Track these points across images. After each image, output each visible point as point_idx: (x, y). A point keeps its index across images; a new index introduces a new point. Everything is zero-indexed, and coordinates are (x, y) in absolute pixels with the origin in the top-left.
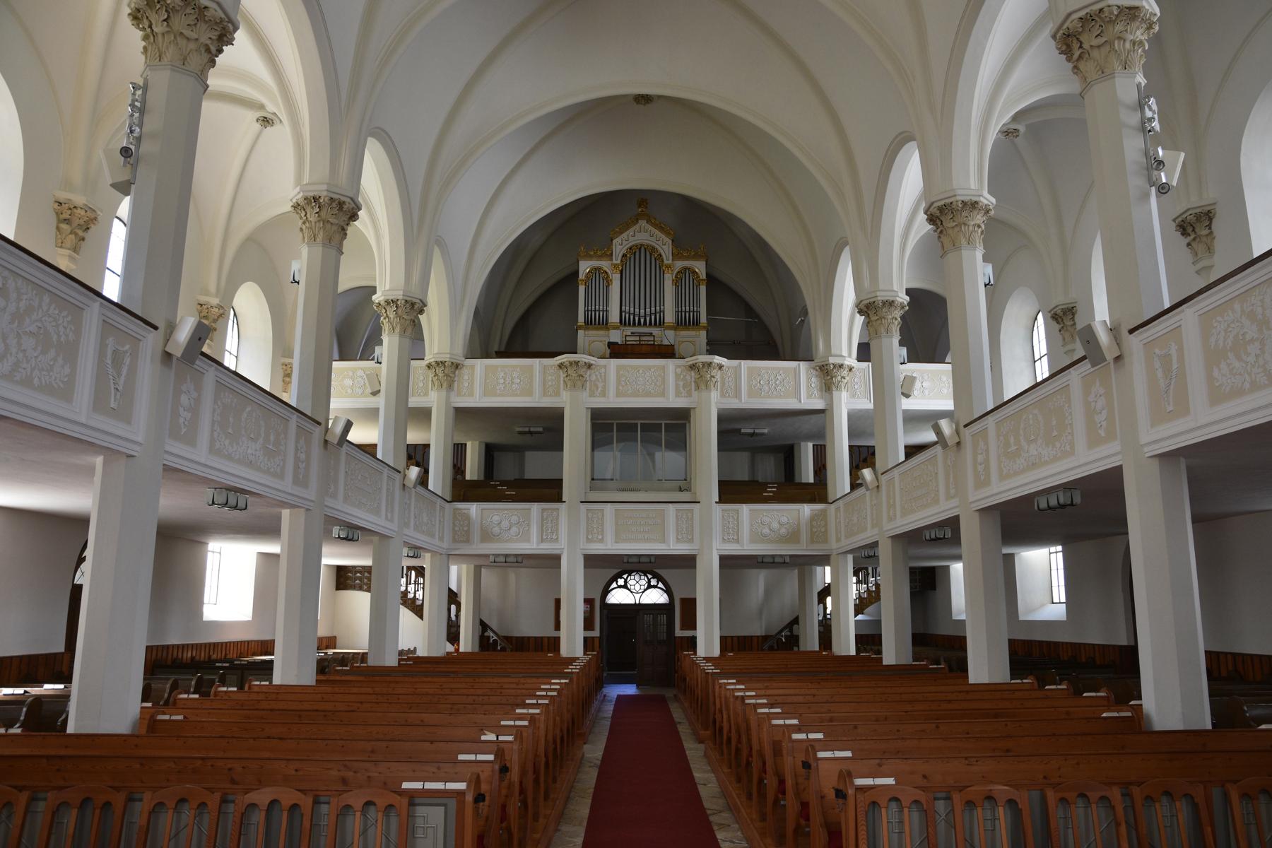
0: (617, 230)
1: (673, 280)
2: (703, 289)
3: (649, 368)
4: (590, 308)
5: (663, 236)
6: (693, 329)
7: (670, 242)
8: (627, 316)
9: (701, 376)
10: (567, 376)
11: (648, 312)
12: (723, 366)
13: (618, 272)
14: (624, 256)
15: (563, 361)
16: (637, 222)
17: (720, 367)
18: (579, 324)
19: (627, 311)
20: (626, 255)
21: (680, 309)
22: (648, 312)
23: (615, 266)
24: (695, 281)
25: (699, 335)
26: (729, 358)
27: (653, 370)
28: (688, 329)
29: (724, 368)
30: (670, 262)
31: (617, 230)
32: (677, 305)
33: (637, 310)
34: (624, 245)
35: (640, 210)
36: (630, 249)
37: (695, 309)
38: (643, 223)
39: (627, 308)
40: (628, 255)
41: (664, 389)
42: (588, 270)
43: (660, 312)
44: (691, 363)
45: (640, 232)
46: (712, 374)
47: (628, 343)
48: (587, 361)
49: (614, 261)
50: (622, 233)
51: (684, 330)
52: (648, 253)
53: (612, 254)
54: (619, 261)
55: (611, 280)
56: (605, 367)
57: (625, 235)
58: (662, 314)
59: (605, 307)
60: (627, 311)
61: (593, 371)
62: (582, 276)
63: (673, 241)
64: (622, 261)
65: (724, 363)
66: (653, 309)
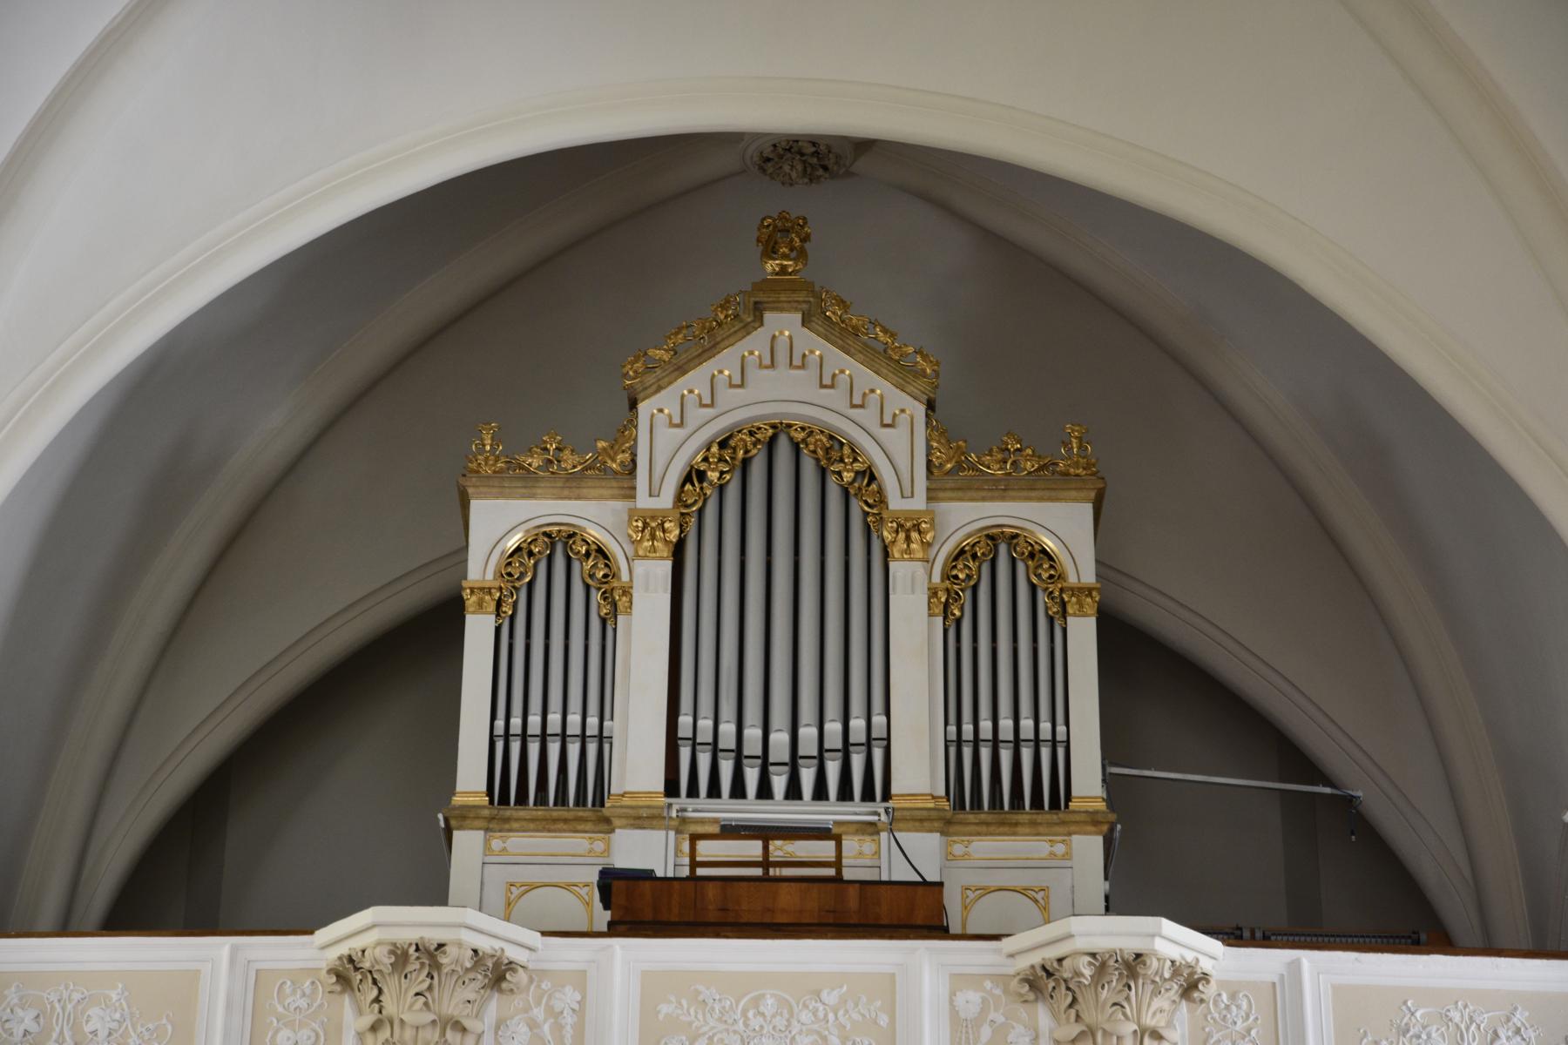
0: (659, 354)
1: (933, 593)
2: (1083, 634)
3: (811, 986)
4: (516, 722)
5: (883, 387)
6: (1035, 829)
7: (920, 410)
8: (704, 760)
9: (1091, 1032)
10: (374, 1028)
11: (808, 744)
12: (1205, 977)
13: (664, 550)
14: (694, 476)
15: (357, 943)
16: (760, 321)
17: (1191, 984)
18: (457, 800)
19: (705, 735)
20: (701, 476)
21: (968, 728)
22: (808, 744)
23: (649, 524)
24: (1042, 598)
25: (1067, 856)
26: (1234, 936)
27: (831, 997)
28: (1011, 828)
29: (1208, 991)
30: (919, 503)
31: (659, 354)
32: (953, 710)
33: (753, 733)
34: (691, 424)
35: (771, 266)
36: (723, 444)
37: (1045, 726)
38: (784, 324)
39: (706, 724)
40: (713, 476)
41: (956, 559)
42: (512, 542)
43: (868, 744)
44: (1036, 959)
45: (773, 365)
46: (1149, 1021)
47: (701, 872)
48: (485, 944)
49: (643, 501)
50: (682, 370)
51: (986, 829)
52: (808, 466)
53: (631, 469)
54: (666, 500)
55: (627, 592)
56: (580, 979)
57: (695, 381)
58: (878, 754)
59: (593, 721)
60: (705, 735)
61: (517, 1001)
62: (481, 567)
63: (931, 406)
64: (679, 499)
65: (1206, 965)
66: (833, 727)
